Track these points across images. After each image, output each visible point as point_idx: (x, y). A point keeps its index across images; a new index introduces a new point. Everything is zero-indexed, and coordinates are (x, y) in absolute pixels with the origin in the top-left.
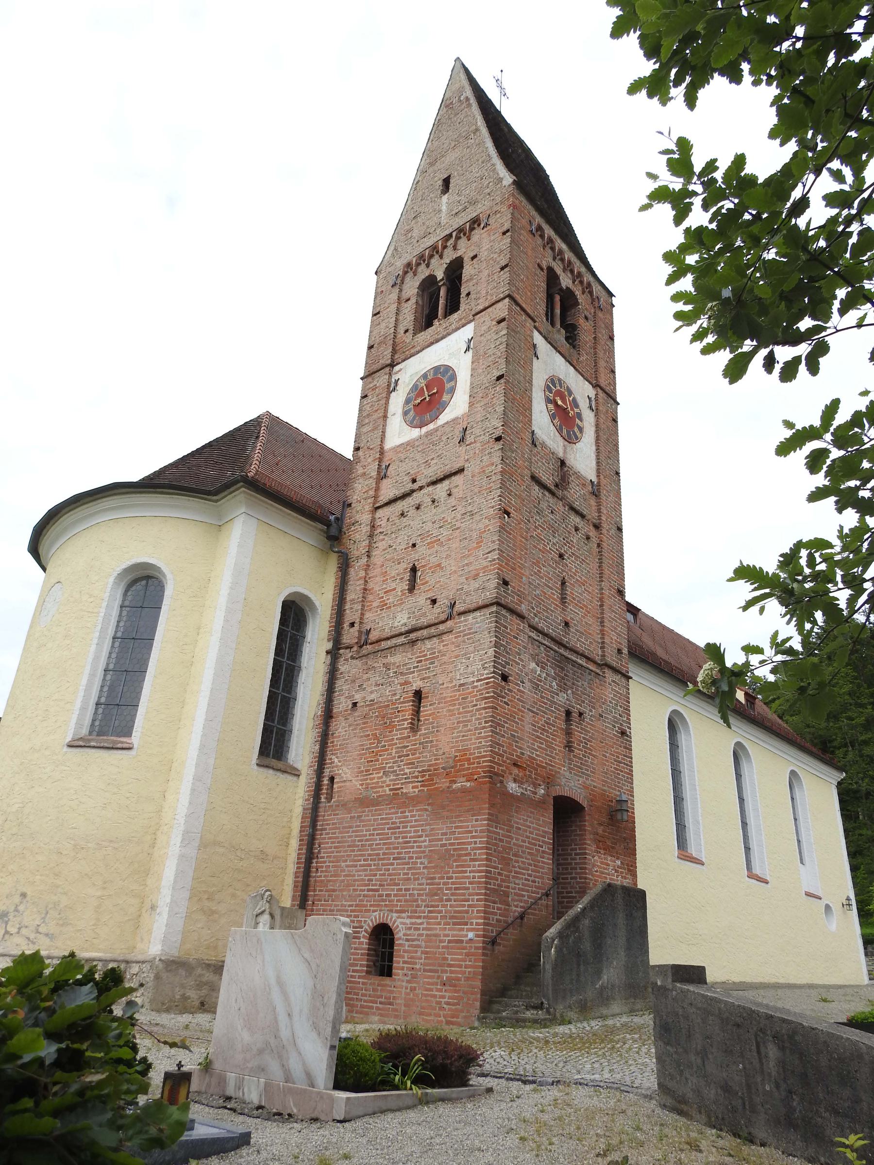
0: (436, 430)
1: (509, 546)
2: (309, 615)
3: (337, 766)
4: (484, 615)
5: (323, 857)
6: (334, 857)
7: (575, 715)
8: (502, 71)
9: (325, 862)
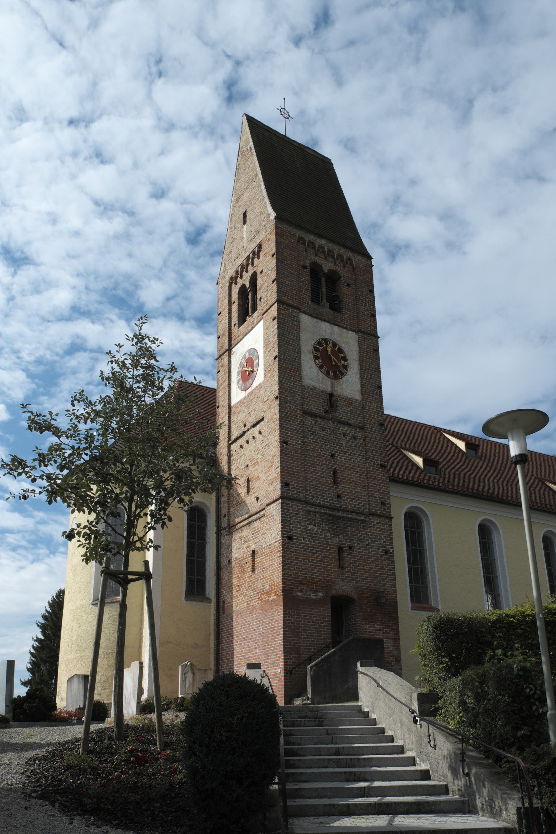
0: (252, 392)
1: (288, 462)
2: (206, 511)
3: (225, 595)
4: (276, 505)
5: (223, 643)
6: (228, 642)
7: (346, 549)
8: (284, 99)
9: (225, 645)
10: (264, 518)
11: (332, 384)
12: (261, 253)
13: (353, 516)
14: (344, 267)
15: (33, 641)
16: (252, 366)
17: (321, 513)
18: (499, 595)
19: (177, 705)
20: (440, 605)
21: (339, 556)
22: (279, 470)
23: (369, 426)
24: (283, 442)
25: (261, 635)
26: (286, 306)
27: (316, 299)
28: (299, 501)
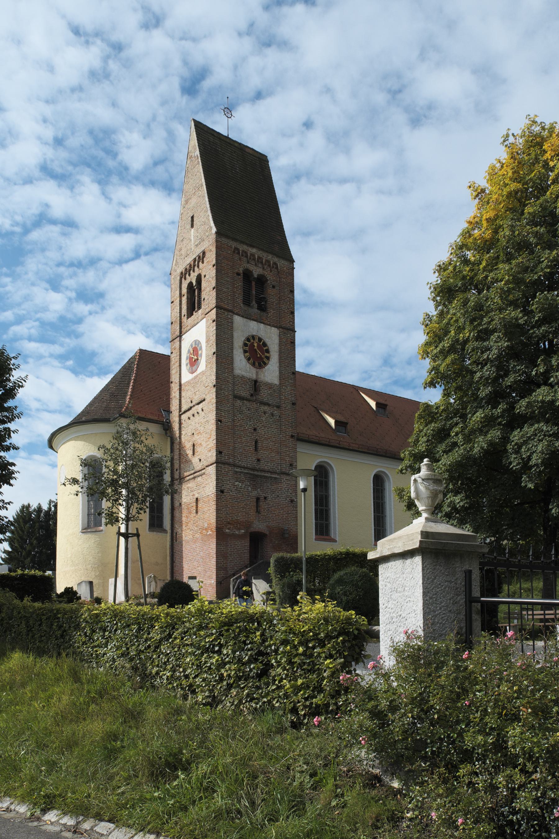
0: (197, 376)
10: (204, 476)
11: (257, 372)
12: (205, 259)
13: (268, 475)
14: (271, 271)
15: (2, 553)
16: (197, 356)
17: (245, 473)
18: (386, 529)
19: (151, 596)
20: (337, 537)
21: (257, 504)
22: (215, 442)
23: (284, 405)
24: (219, 421)
25: (202, 557)
26: (222, 311)
27: (247, 302)
28: (229, 464)
